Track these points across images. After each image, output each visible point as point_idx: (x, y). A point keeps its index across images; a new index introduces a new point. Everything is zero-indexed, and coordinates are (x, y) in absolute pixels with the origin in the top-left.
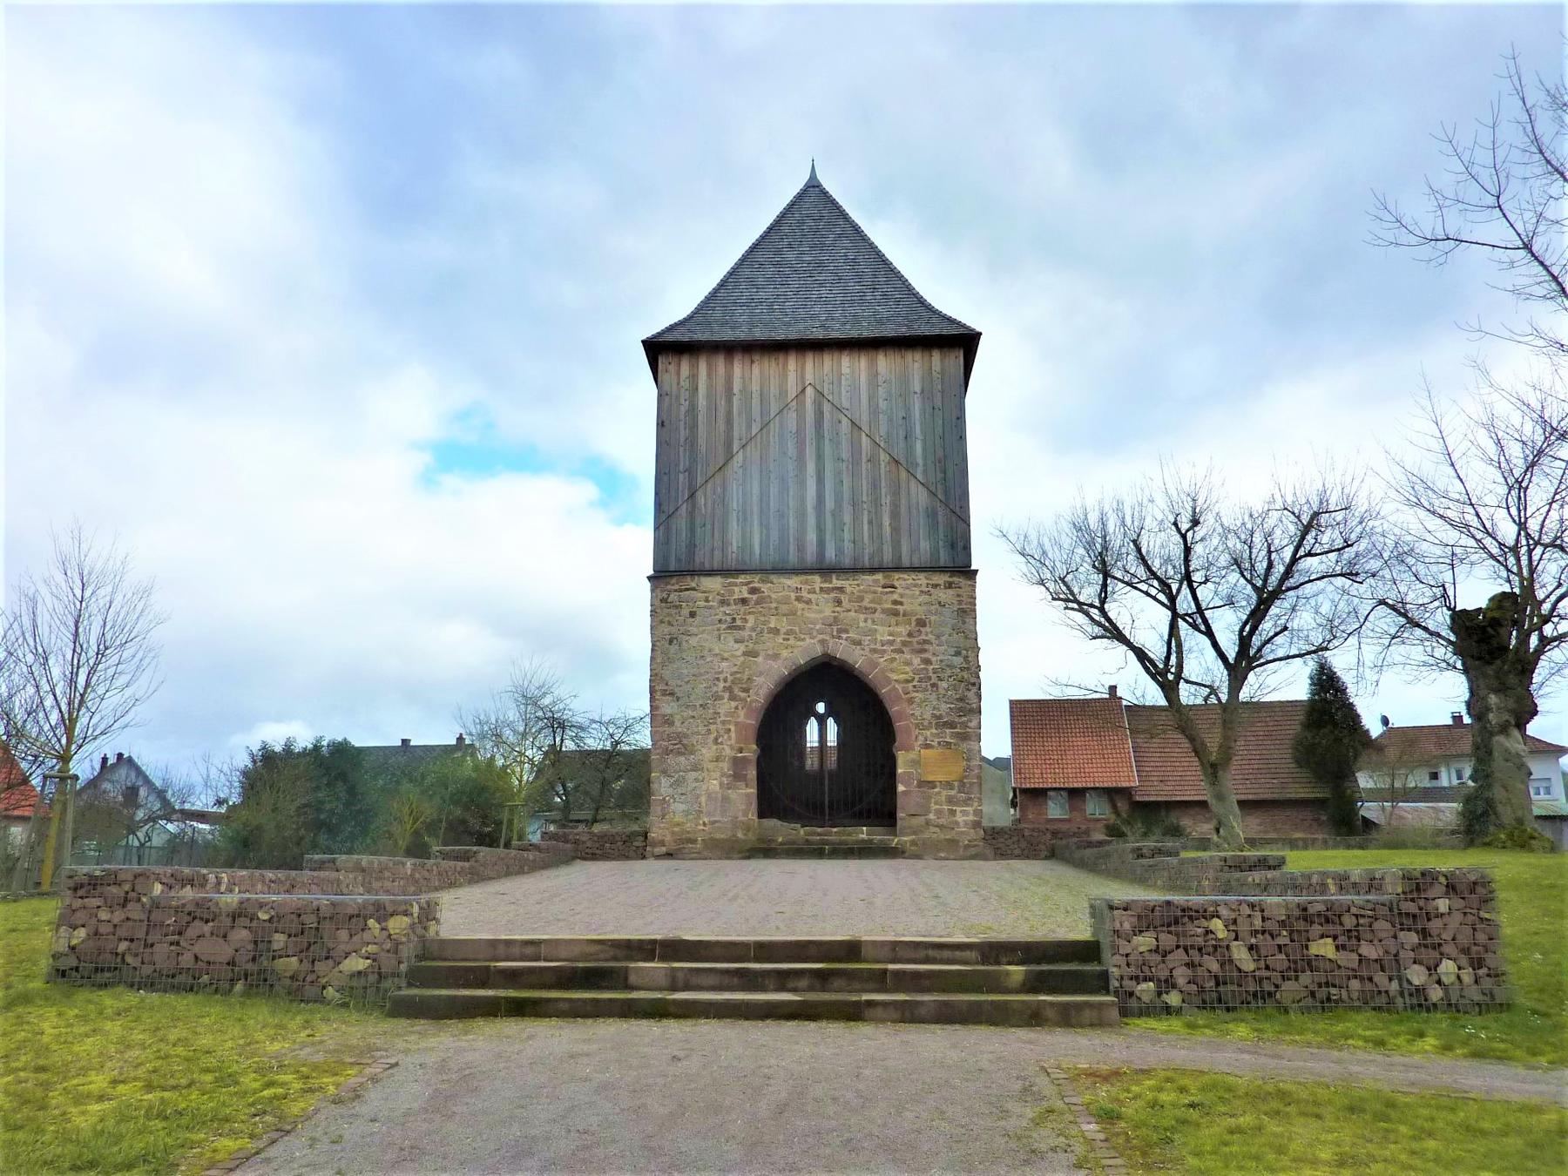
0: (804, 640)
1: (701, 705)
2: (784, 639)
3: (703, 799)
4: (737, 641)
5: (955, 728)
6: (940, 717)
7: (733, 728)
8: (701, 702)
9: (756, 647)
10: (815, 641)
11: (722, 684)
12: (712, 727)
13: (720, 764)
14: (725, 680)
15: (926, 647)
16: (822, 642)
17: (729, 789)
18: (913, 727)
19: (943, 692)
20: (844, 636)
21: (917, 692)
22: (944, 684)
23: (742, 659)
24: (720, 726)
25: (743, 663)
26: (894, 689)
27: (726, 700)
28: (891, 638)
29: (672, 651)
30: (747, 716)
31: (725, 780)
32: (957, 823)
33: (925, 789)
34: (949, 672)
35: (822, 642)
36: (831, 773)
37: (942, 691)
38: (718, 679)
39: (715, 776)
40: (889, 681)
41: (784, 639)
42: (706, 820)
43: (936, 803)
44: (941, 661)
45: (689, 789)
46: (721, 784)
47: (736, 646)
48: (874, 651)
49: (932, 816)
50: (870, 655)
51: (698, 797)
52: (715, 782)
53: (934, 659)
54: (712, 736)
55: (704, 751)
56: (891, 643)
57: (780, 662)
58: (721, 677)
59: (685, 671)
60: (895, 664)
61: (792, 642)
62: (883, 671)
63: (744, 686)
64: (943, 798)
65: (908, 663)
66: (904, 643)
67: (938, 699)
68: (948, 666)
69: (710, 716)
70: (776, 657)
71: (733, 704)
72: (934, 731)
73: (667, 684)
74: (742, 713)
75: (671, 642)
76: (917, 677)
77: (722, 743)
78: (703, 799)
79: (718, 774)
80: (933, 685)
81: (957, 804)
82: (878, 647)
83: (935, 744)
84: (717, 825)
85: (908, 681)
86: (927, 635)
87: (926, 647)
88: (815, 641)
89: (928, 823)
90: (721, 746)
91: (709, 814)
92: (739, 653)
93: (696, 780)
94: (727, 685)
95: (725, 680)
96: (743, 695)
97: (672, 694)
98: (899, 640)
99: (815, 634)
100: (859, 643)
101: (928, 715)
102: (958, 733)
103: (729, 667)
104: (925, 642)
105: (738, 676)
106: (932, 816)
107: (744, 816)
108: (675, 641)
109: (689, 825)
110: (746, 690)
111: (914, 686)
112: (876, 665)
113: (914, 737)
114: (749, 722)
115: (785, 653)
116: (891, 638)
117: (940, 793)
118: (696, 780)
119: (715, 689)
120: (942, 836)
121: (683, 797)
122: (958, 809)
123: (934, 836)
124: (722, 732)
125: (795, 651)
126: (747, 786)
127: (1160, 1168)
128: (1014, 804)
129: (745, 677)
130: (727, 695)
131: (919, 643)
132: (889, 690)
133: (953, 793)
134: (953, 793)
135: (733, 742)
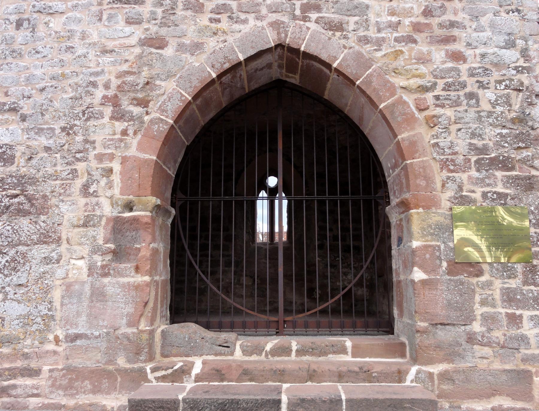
0: (245, 21)
1: (63, 129)
2: (211, 20)
3: (57, 295)
4: (129, 22)
5: (512, 169)
6: (484, 150)
7: (116, 166)
8: (62, 124)
9: (163, 31)
10: (265, 23)
11: (100, 93)
12: (81, 166)
13: (91, 232)
14: (107, 86)
15: (456, 32)
16: (276, 25)
17: (105, 275)
18: (436, 167)
19: (488, 107)
20: (314, 16)
21: (443, 106)
22: (489, 95)
23: (137, 50)
24: (94, 164)
25: (140, 57)
26: (401, 102)
27: (106, 119)
28: (394, 19)
29: (20, 40)
30: (141, 147)
31: (99, 260)
32: (524, 339)
33: (113, 122)
34: (496, 75)
35: (276, 25)
36: (284, 243)
37: (485, 106)
38: (94, 84)
39: (79, 254)
40: (392, 90)
41: (211, 20)
42: (61, 333)
43: (483, 303)
44: (483, 56)
45: (34, 275)
46: (91, 269)
47: (128, 29)
48: (365, 40)
49: (477, 327)
50: (357, 47)
51: (47, 291)
52: (81, 263)
53: (469, 53)
54: (79, 183)
55: (64, 208)
56: (395, 26)
57: (204, 57)
58: (101, 80)
59: (38, 72)
60: (400, 62)
61: (224, 24)
62: (382, 73)
63: (140, 95)
64: (497, 295)
65: (423, 60)
66: (417, 27)
67: (479, 119)
68: (496, 65)
69: (80, 147)
70: (197, 47)
71: (119, 126)
72: (474, 173)
73: (6, 94)
74: (134, 142)
75: (19, 25)
76: (441, 83)
77: (95, 194)
78: (57, 295)
79: (85, 250)
80: (471, 96)
81: (524, 304)
82: (372, 33)
83: (477, 196)
84: (78, 342)
85: (424, 89)
86: (455, 14)
87: (456, 32)
88: (265, 23)
89: (471, 339)
90: (94, 200)
91: (67, 322)
92: (133, 40)
93: (47, 260)
94: (110, 93)
95: (107, 86)
96: (137, 110)
97: (14, 110)
98: (407, 22)
99: (264, 11)
100: (339, 27)
101: (462, 146)
102: (517, 178)
103: (114, 63)
104: (452, 24)
105: (130, 78)
106: (477, 327)
107: (130, 324)
108: (26, 24)
109: (28, 342)
110: (144, 103)
111: (437, 98)
112: (368, 63)
113: (439, 185)
114: (147, 156)
115: (212, 44)
116: (394, 19)
117: (489, 284)
118: (47, 260)
119: (88, 100)
120: (497, 366)
121: (23, 290)
122: (527, 314)
123: (483, 364)
124: (96, 175)
125: (230, 39)
126: (137, 269)
127: (489, 222)
128: (319, 399)
129: (142, 81)
130: (108, 111)
131: (441, 26)
132: (393, 105)
133: (513, 284)
134: (513, 284)
135: (116, 191)
